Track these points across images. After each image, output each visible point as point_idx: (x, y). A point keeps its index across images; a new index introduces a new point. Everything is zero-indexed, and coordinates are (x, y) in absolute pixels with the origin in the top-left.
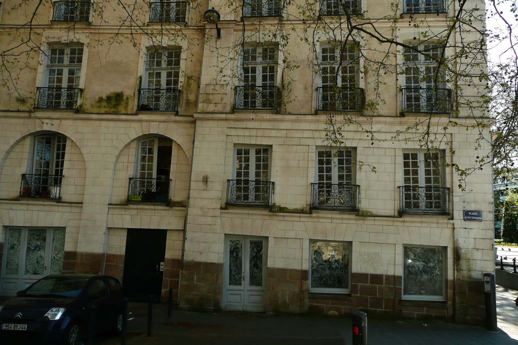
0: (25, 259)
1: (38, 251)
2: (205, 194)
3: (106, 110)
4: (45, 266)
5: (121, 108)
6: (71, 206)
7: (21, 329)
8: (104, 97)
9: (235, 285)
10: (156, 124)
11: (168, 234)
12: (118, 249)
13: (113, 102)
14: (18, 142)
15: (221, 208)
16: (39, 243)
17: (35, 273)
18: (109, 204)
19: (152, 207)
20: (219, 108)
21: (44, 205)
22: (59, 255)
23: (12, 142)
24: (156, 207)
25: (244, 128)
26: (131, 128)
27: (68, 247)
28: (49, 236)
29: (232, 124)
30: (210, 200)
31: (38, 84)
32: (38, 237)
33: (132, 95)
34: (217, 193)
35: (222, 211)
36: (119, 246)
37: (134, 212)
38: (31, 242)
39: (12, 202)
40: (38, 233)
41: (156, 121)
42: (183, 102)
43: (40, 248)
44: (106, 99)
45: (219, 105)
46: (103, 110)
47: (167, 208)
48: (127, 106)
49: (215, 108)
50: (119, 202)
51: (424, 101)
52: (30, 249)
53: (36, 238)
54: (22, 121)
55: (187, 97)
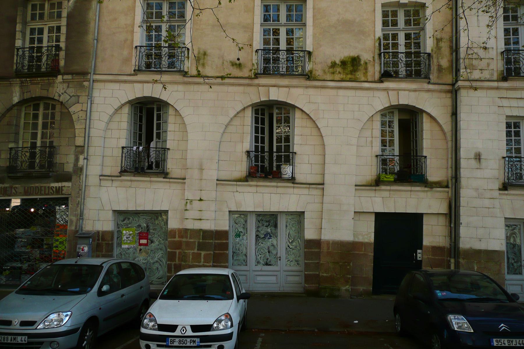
0: (254, 247)
1: (269, 239)
2: (478, 173)
3: (342, 76)
4: (279, 255)
5: (360, 75)
6: (309, 188)
7: (518, 345)
8: (338, 62)
9: (514, 274)
10: (407, 93)
11: (425, 219)
12: (366, 236)
13: (349, 68)
14: (117, 111)
15: (500, 190)
16: (269, 230)
17: (267, 264)
18: (100, 176)
19: (409, 188)
20: (486, 75)
21: (277, 187)
22: (294, 244)
23: (232, 113)
24: (413, 188)
25: (517, 98)
26: (378, 98)
27: (310, 234)
28: (282, 222)
29: (504, 93)
30: (486, 180)
31: (137, 43)
32: (267, 223)
33: (371, 59)
34: (493, 170)
35: (501, 192)
36: (367, 232)
37: (386, 194)
38: (260, 229)
39: (238, 183)
40: (269, 220)
41: (404, 90)
42: (434, 68)
43: (271, 236)
44: (340, 64)
45: (484, 72)
46: (337, 77)
47: (426, 189)
48: (366, 72)
49: (481, 75)
50: (364, 183)
51: (403, 65)
52: (260, 237)
53: (266, 224)
54: (241, 88)
55: (438, 62)
